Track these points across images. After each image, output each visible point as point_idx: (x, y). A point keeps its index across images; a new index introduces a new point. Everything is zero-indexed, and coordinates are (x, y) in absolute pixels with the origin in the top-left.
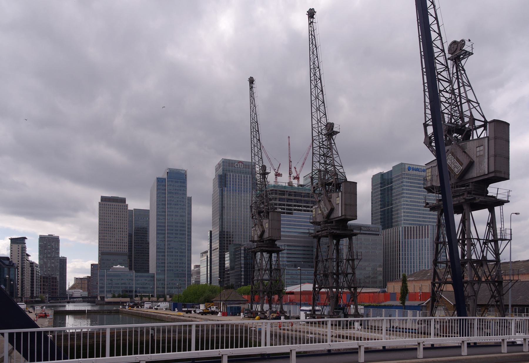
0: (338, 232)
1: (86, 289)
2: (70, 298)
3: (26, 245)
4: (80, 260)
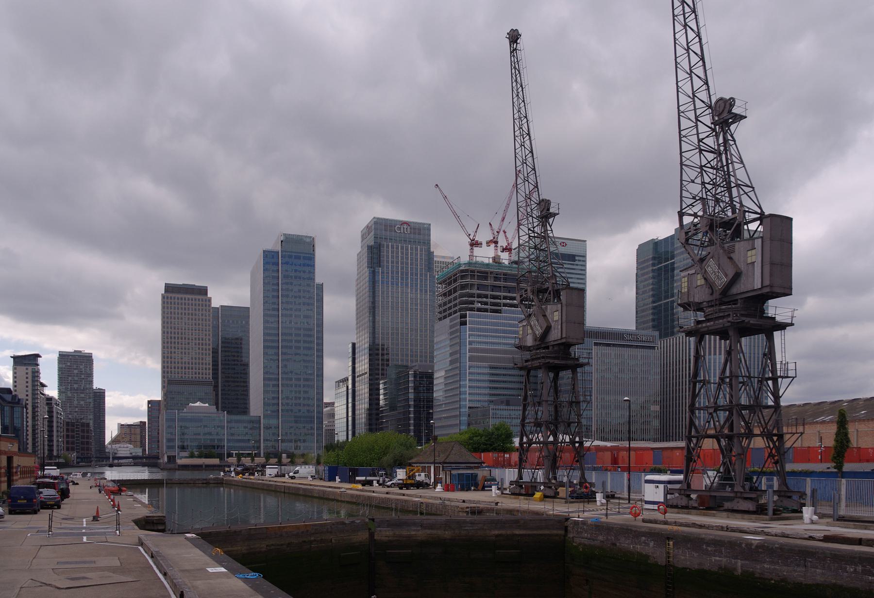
0: (556, 362)
1: (139, 443)
2: (114, 458)
3: (40, 367)
4: (130, 393)
